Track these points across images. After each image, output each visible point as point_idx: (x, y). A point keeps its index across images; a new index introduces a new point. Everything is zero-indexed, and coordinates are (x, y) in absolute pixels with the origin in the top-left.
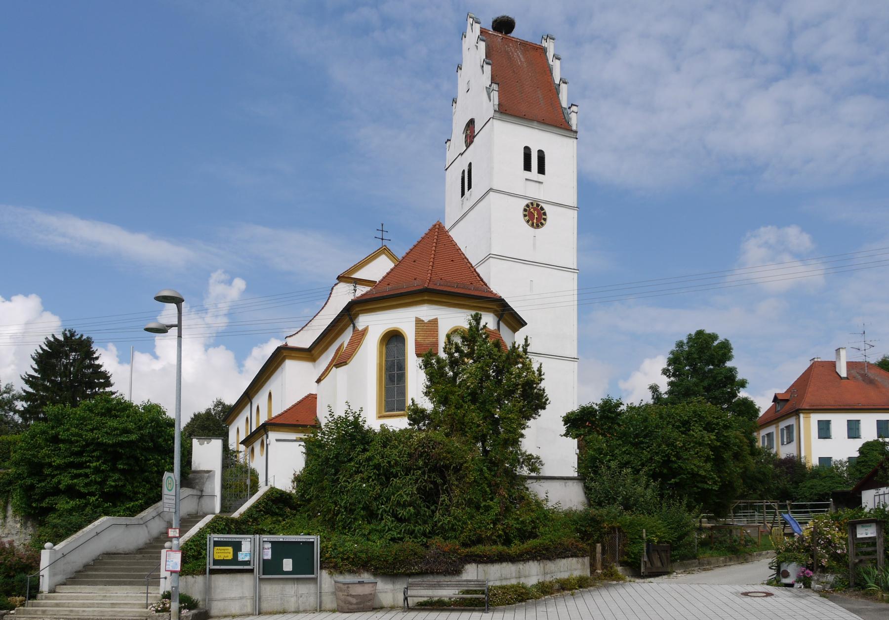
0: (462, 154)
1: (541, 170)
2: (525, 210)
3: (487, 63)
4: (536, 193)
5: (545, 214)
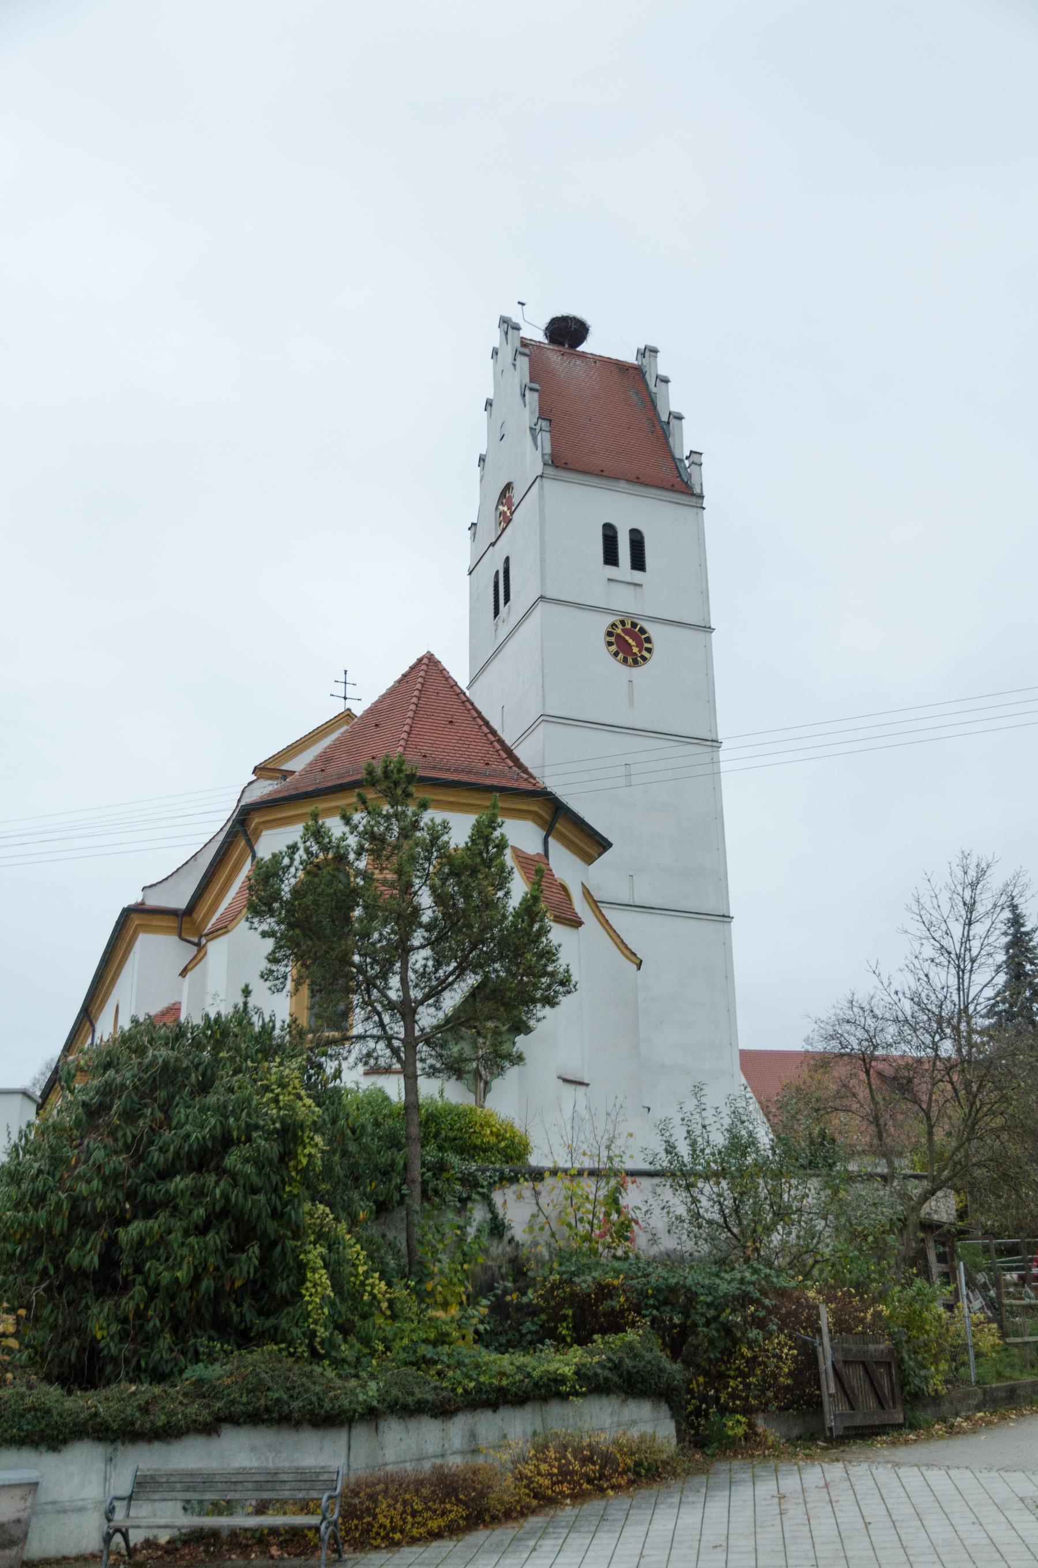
0: (493, 544)
1: (638, 562)
2: (609, 634)
3: (531, 389)
4: (626, 602)
5: (648, 640)
